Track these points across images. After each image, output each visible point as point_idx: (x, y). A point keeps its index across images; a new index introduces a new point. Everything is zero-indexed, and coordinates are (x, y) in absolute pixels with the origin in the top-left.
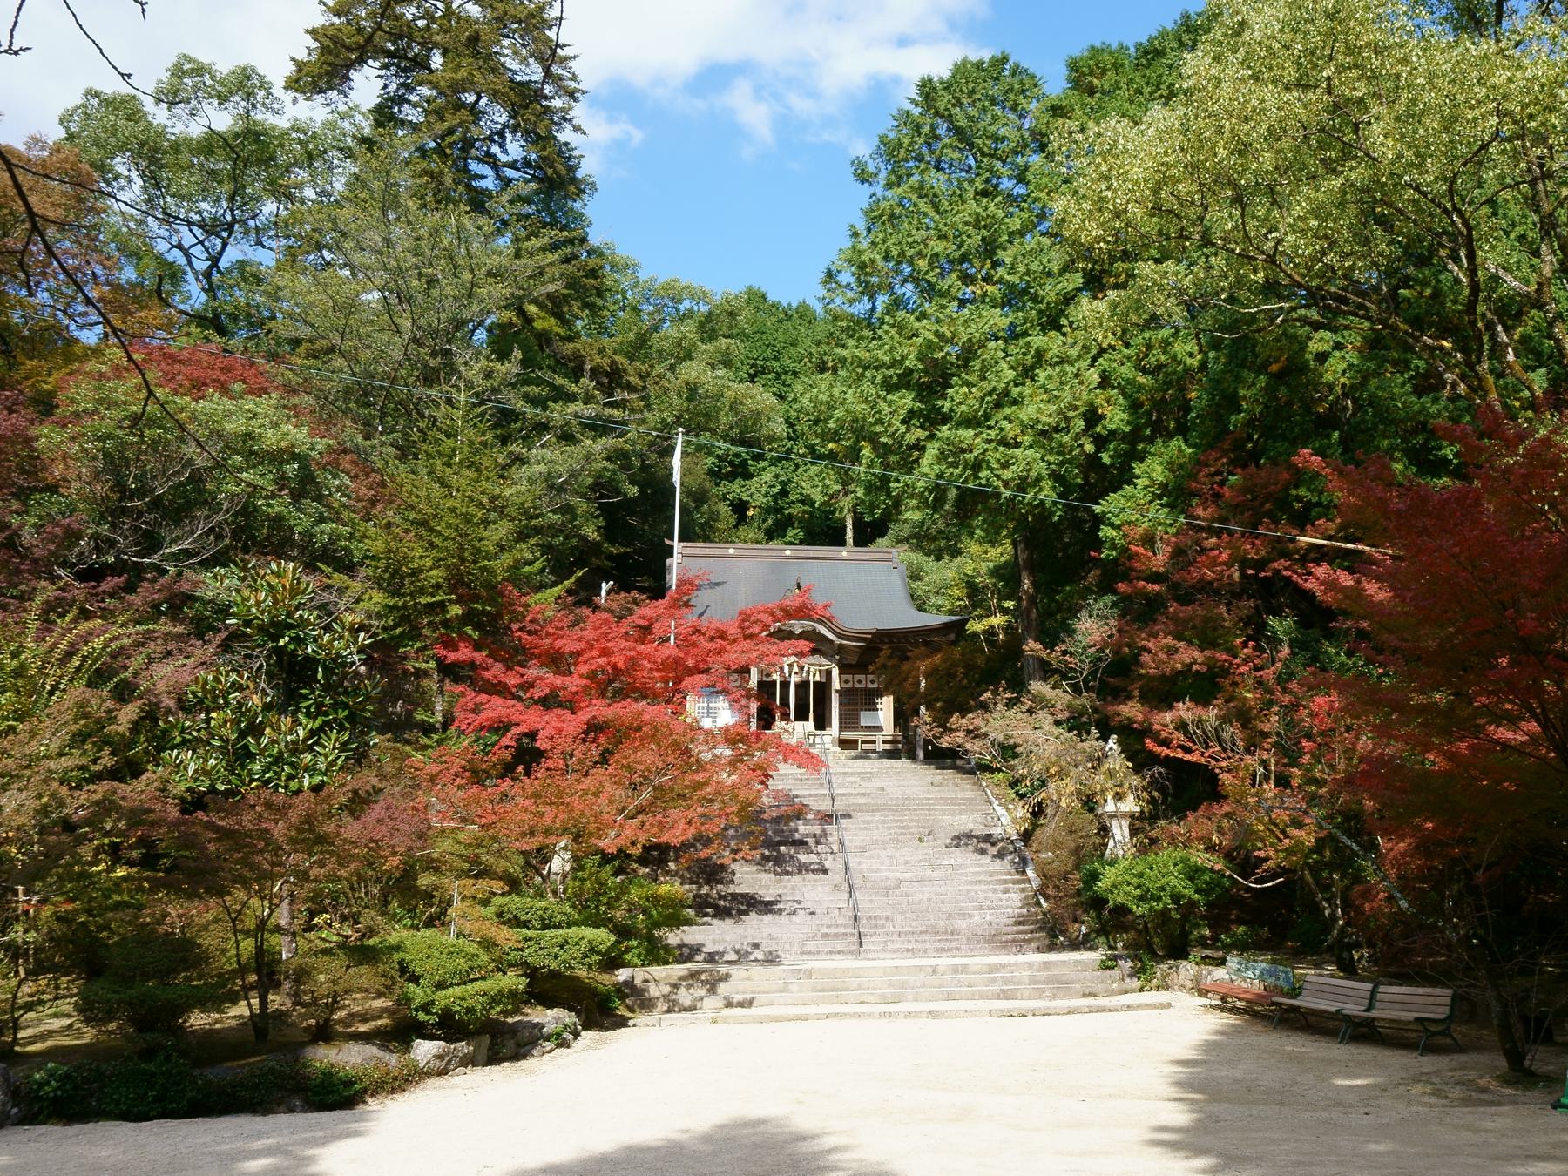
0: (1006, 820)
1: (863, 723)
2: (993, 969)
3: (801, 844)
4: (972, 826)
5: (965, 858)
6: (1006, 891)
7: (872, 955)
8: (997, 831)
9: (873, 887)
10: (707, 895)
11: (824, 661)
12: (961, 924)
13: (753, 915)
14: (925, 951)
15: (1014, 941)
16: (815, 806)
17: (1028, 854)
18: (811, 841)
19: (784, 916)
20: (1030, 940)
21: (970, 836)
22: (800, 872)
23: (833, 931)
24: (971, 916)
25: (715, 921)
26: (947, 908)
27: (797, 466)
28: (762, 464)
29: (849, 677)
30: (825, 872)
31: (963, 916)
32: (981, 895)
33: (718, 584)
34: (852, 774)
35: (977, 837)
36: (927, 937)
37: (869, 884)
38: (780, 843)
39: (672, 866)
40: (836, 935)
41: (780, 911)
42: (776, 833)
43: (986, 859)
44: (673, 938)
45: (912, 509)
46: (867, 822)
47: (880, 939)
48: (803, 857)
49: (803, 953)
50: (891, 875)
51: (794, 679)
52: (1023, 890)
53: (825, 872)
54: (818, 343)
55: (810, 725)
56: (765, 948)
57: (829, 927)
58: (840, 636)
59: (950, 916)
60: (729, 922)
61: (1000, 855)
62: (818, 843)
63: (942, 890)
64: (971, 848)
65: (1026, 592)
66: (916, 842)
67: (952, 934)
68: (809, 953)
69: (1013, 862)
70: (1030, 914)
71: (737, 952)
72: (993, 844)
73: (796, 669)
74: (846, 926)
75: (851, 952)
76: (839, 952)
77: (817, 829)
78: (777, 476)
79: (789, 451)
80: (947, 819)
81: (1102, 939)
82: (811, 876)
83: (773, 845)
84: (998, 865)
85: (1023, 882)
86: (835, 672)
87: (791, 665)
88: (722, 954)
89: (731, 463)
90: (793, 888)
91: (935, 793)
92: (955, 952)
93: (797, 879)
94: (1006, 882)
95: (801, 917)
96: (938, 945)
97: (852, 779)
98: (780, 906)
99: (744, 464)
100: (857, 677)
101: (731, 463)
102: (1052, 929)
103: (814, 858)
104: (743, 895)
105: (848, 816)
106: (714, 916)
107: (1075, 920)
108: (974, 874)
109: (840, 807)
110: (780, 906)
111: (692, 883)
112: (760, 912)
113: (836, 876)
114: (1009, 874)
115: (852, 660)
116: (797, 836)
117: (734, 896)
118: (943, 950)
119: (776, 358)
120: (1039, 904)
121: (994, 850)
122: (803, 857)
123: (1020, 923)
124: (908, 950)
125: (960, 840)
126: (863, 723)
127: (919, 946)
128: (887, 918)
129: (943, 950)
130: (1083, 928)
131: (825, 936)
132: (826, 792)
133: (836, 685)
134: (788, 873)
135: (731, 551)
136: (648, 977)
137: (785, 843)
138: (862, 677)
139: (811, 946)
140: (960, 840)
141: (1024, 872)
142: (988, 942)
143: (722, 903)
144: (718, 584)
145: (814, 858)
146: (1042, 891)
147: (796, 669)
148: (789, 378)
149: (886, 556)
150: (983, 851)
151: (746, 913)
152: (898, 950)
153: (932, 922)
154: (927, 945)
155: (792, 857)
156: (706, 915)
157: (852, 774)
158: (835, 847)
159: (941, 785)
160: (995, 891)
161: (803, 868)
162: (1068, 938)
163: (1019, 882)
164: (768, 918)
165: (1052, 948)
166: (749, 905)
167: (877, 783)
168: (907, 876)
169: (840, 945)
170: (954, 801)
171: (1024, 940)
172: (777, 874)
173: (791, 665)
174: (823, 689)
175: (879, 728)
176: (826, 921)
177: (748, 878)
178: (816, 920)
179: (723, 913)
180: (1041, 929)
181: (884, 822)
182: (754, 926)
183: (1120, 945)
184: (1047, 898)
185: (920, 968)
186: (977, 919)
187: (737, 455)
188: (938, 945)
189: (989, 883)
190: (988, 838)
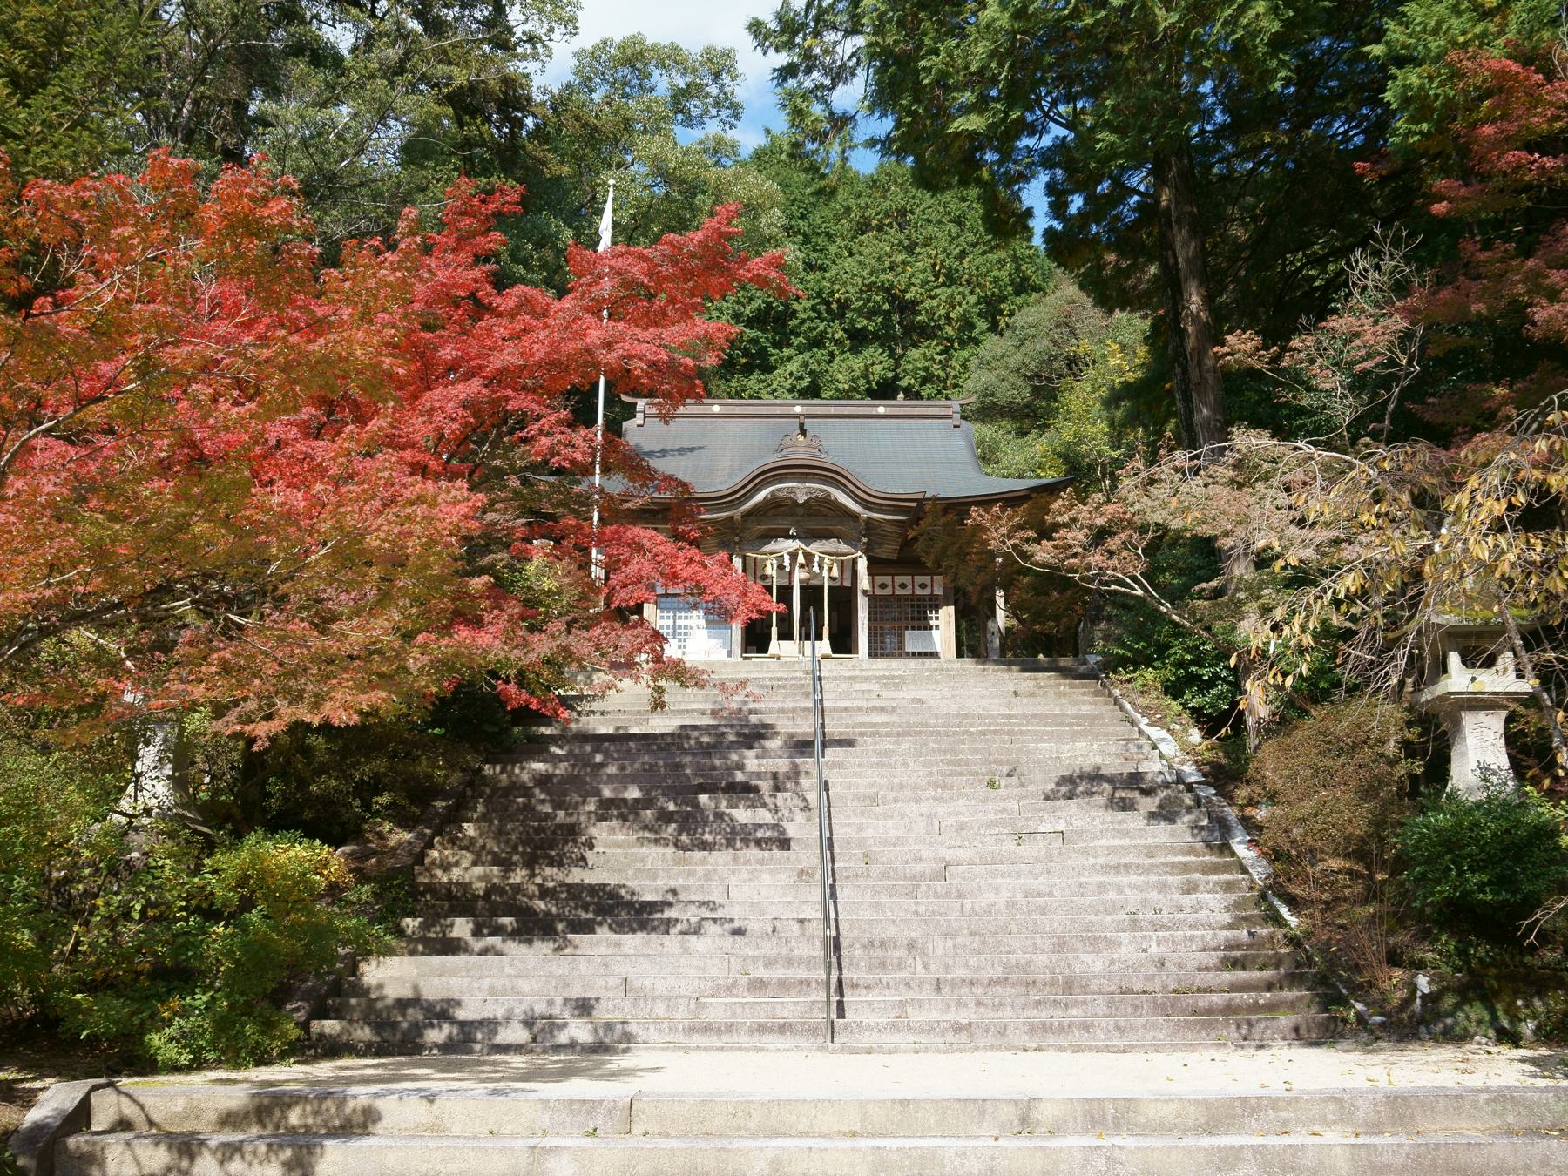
0: (1169, 747)
1: (909, 648)
2: (1221, 1115)
3: (745, 791)
4: (1098, 760)
5: (1087, 817)
6: (1190, 889)
7: (866, 1039)
8: (1152, 768)
9: (886, 875)
10: (517, 889)
11: (844, 548)
12: (1091, 963)
13: (603, 933)
14: (1002, 1031)
15: (1229, 1009)
16: (785, 726)
17: (1232, 813)
18: (765, 785)
19: (672, 941)
20: (1271, 1007)
21: (1096, 777)
22: (730, 844)
23: (780, 973)
24: (1112, 944)
25: (512, 946)
26: (1055, 923)
27: (832, 355)
28: (786, 352)
29: (887, 579)
30: (784, 844)
31: (1095, 942)
32: (1133, 898)
33: (691, 450)
34: (866, 679)
35: (1110, 780)
36: (1007, 993)
37: (875, 870)
38: (702, 789)
39: (470, 829)
40: (783, 983)
41: (668, 924)
42: (699, 771)
43: (1135, 821)
44: (391, 975)
45: (966, 110)
46: (886, 753)
47: (893, 997)
48: (742, 815)
49: (691, 1030)
50: (926, 852)
51: (800, 575)
52: (1229, 887)
53: (784, 844)
54: (859, 195)
55: (824, 646)
56: (602, 1014)
57: (770, 963)
58: (867, 505)
59: (1060, 945)
60: (543, 947)
61: (1166, 814)
62: (777, 788)
63: (1041, 883)
64: (1101, 800)
65: (1195, 319)
66: (982, 789)
67: (1068, 986)
68: (707, 1029)
69: (1195, 827)
70: (1255, 942)
71: (529, 1023)
72: (1147, 792)
73: (801, 559)
74: (809, 963)
75: (812, 1031)
76: (783, 1029)
77: (782, 765)
78: (805, 365)
79: (823, 335)
80: (1047, 748)
81: (1476, 1011)
82: (753, 852)
83: (687, 792)
84: (1161, 833)
85: (1226, 868)
86: (862, 564)
87: (793, 556)
88: (491, 1025)
89: (746, 352)
90: (708, 876)
91: (1024, 706)
92: (1079, 1037)
93: (720, 858)
94: (1186, 868)
95: (712, 939)
96: (1043, 1015)
97: (865, 686)
98: (669, 914)
99: (763, 353)
100: (899, 579)
101: (746, 352)
102: (1322, 980)
103: (765, 816)
104: (594, 890)
105: (848, 743)
106: (515, 934)
107: (1394, 959)
108: (1111, 850)
109: (834, 728)
110: (669, 914)
111: (497, 861)
112: (619, 927)
113: (806, 854)
114: (1191, 851)
115: (889, 551)
116: (740, 777)
117: (575, 891)
118: (1046, 1028)
119: (802, 217)
120: (1277, 920)
121: (1151, 804)
122: (742, 815)
123: (1236, 964)
124: (958, 1028)
125: (1074, 785)
126: (909, 648)
127: (987, 1015)
128: (912, 946)
129: (1046, 1028)
130: (1423, 983)
131: (758, 985)
132: (810, 704)
133: (864, 582)
134: (705, 846)
135: (716, 409)
136: (129, 1110)
137: (710, 789)
138: (907, 579)
139: (717, 1012)
140: (1074, 785)
141: (1225, 848)
142: (1164, 1010)
143: (540, 905)
144: (691, 450)
145: (765, 816)
146: (1277, 888)
147: (801, 559)
148: (821, 240)
149: (943, 412)
150: (1126, 806)
151: (587, 928)
152: (932, 1028)
153: (1018, 957)
154: (1007, 1015)
155: (719, 816)
156: (497, 931)
157: (866, 679)
158: (812, 797)
159: (1033, 694)
160: (1163, 887)
161: (739, 837)
162: (1380, 1005)
163: (1216, 869)
164: (632, 941)
165: (1327, 1033)
166: (603, 911)
167: (908, 693)
168: (961, 854)
169: (789, 1009)
170: (1059, 720)
171: (1255, 1008)
172: (678, 845)
173: (793, 556)
174: (844, 598)
175: (934, 655)
176: (768, 949)
177: (617, 856)
178: (742, 945)
179: (533, 927)
180: (1294, 979)
181: (919, 754)
182: (602, 961)
183: (1527, 1028)
184: (1293, 902)
185: (979, 1108)
186: (1127, 951)
187: (755, 341)
188: (1043, 1015)
189: (1148, 870)
190: (1135, 781)
